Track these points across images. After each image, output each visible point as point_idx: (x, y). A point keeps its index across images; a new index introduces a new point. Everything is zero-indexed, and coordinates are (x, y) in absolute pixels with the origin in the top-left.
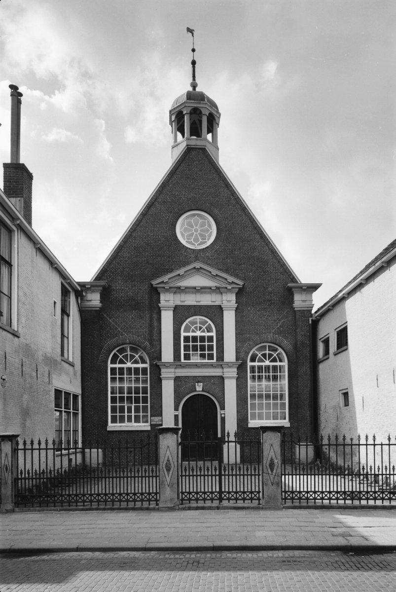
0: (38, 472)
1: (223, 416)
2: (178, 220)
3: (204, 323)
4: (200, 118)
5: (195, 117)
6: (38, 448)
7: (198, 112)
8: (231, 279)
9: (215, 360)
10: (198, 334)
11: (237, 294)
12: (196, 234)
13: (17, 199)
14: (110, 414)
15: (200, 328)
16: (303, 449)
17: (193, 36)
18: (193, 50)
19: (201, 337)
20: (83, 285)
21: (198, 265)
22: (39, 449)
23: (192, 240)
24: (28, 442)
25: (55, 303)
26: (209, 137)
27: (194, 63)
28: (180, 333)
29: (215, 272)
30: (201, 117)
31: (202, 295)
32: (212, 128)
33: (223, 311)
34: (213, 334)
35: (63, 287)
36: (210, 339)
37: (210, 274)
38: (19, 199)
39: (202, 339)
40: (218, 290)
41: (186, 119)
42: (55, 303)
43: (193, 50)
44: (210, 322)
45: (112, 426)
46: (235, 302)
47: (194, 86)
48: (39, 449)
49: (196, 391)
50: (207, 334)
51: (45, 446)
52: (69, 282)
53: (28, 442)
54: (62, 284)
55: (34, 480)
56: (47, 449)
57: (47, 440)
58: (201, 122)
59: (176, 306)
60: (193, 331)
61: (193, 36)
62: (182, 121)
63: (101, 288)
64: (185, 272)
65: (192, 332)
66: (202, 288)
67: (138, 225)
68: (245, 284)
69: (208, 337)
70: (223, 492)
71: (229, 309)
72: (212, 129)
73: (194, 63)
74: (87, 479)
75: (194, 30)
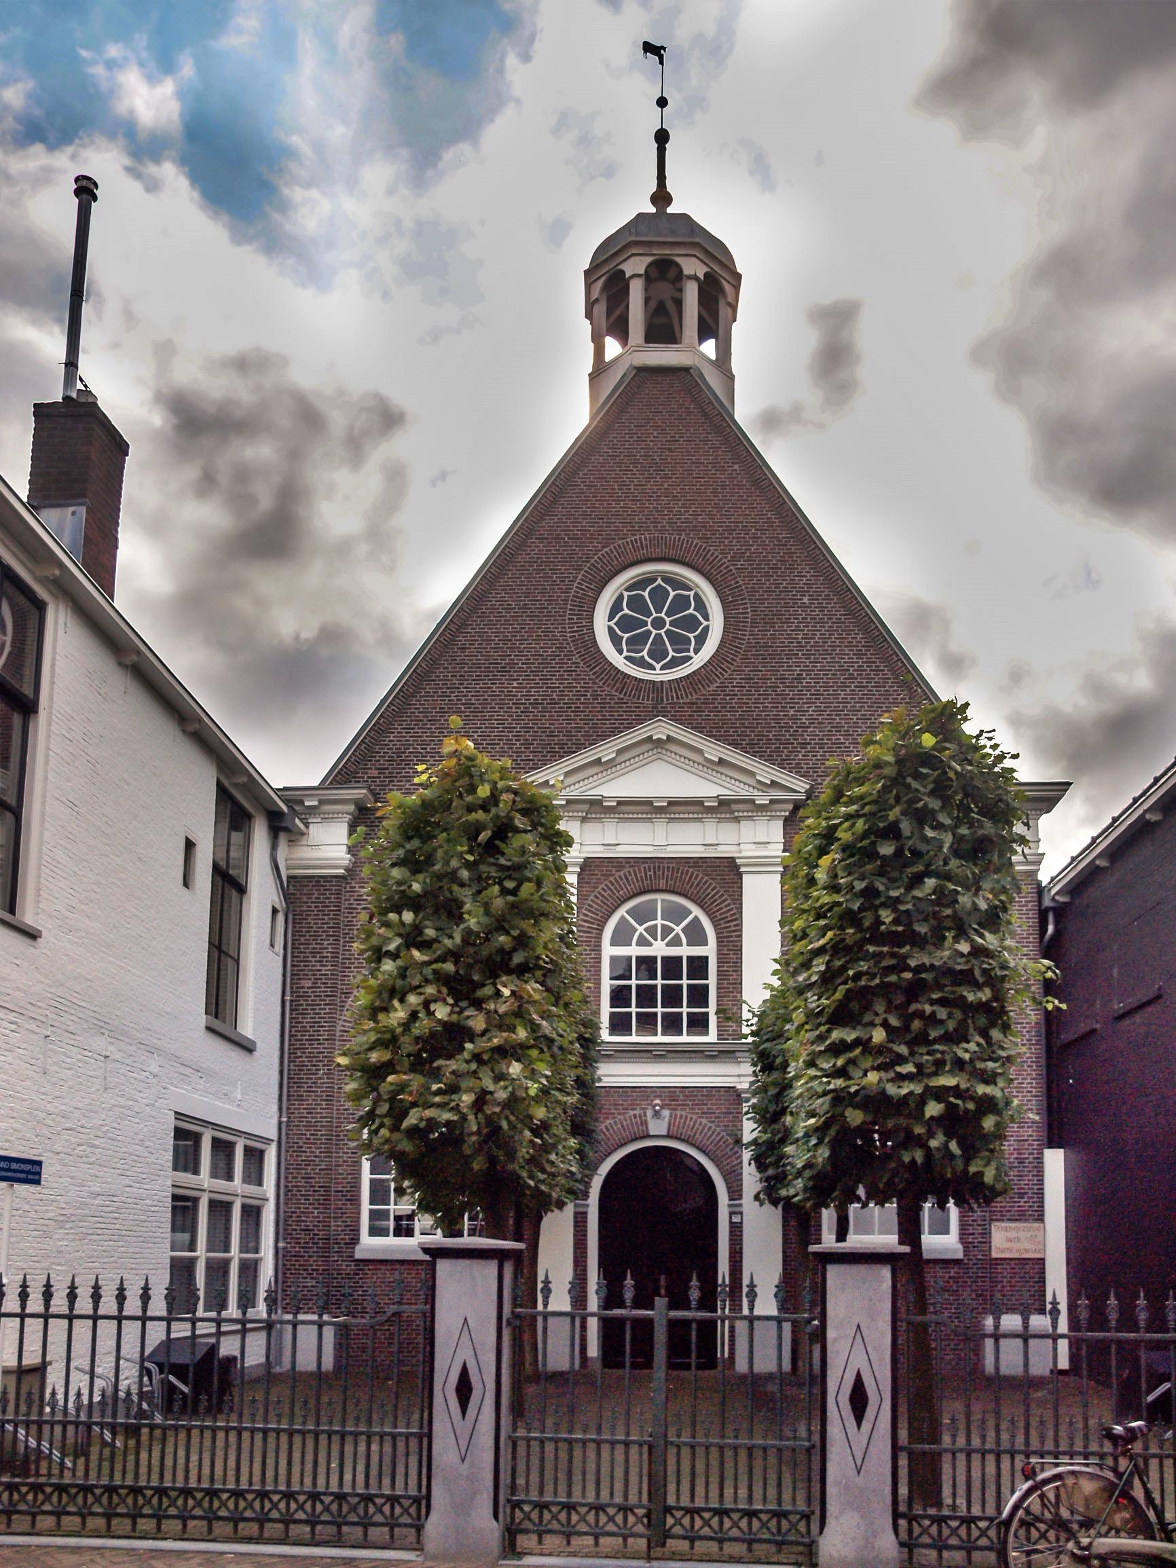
0: (86, 1402)
1: (736, 1219)
2: (603, 587)
3: (675, 914)
4: (677, 295)
5: (664, 290)
6: (91, 1312)
7: (672, 274)
8: (766, 772)
9: (712, 1037)
10: (659, 949)
11: (787, 822)
12: (649, 614)
13: (65, 510)
14: (366, 1207)
15: (667, 931)
16: (307, 1336)
17: (661, 62)
18: (662, 102)
19: (666, 960)
20: (293, 796)
21: (661, 729)
22: (71, 1318)
23: (645, 653)
24: (84, 1294)
25: (190, 845)
26: (709, 348)
27: (662, 137)
28: (598, 948)
29: (714, 750)
30: (681, 290)
31: (674, 826)
32: (716, 320)
33: (740, 875)
34: (709, 950)
35: (223, 794)
36: (698, 966)
37: (700, 760)
38: (72, 509)
39: (672, 966)
40: (725, 809)
41: (636, 292)
42: (190, 845)
43: (662, 102)
44: (696, 912)
45: (370, 1244)
46: (781, 847)
47: (661, 197)
48: (95, 1318)
49: (648, 1136)
50: (685, 951)
51: (42, 1302)
52: (244, 785)
53: (84, 1294)
54: (219, 785)
55: (71, 1429)
56: (95, 1318)
57: (24, 1286)
58: (679, 303)
59: (587, 860)
60: (642, 942)
61: (661, 62)
62: (624, 305)
63: (351, 808)
64: (619, 752)
65: (638, 944)
66: (673, 803)
67: (474, 610)
68: (812, 787)
69: (691, 959)
70: (668, 1510)
71: (761, 865)
72: (712, 325)
73: (662, 137)
74: (227, 1432)
75: (664, 49)
